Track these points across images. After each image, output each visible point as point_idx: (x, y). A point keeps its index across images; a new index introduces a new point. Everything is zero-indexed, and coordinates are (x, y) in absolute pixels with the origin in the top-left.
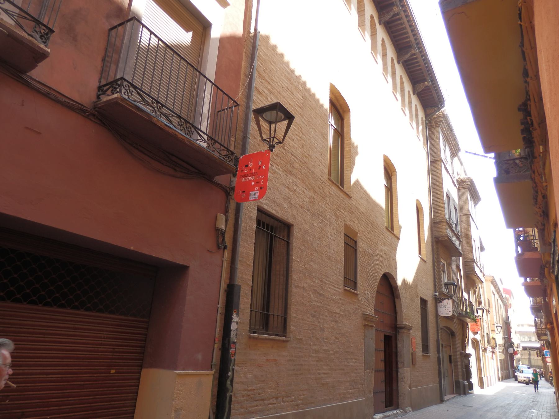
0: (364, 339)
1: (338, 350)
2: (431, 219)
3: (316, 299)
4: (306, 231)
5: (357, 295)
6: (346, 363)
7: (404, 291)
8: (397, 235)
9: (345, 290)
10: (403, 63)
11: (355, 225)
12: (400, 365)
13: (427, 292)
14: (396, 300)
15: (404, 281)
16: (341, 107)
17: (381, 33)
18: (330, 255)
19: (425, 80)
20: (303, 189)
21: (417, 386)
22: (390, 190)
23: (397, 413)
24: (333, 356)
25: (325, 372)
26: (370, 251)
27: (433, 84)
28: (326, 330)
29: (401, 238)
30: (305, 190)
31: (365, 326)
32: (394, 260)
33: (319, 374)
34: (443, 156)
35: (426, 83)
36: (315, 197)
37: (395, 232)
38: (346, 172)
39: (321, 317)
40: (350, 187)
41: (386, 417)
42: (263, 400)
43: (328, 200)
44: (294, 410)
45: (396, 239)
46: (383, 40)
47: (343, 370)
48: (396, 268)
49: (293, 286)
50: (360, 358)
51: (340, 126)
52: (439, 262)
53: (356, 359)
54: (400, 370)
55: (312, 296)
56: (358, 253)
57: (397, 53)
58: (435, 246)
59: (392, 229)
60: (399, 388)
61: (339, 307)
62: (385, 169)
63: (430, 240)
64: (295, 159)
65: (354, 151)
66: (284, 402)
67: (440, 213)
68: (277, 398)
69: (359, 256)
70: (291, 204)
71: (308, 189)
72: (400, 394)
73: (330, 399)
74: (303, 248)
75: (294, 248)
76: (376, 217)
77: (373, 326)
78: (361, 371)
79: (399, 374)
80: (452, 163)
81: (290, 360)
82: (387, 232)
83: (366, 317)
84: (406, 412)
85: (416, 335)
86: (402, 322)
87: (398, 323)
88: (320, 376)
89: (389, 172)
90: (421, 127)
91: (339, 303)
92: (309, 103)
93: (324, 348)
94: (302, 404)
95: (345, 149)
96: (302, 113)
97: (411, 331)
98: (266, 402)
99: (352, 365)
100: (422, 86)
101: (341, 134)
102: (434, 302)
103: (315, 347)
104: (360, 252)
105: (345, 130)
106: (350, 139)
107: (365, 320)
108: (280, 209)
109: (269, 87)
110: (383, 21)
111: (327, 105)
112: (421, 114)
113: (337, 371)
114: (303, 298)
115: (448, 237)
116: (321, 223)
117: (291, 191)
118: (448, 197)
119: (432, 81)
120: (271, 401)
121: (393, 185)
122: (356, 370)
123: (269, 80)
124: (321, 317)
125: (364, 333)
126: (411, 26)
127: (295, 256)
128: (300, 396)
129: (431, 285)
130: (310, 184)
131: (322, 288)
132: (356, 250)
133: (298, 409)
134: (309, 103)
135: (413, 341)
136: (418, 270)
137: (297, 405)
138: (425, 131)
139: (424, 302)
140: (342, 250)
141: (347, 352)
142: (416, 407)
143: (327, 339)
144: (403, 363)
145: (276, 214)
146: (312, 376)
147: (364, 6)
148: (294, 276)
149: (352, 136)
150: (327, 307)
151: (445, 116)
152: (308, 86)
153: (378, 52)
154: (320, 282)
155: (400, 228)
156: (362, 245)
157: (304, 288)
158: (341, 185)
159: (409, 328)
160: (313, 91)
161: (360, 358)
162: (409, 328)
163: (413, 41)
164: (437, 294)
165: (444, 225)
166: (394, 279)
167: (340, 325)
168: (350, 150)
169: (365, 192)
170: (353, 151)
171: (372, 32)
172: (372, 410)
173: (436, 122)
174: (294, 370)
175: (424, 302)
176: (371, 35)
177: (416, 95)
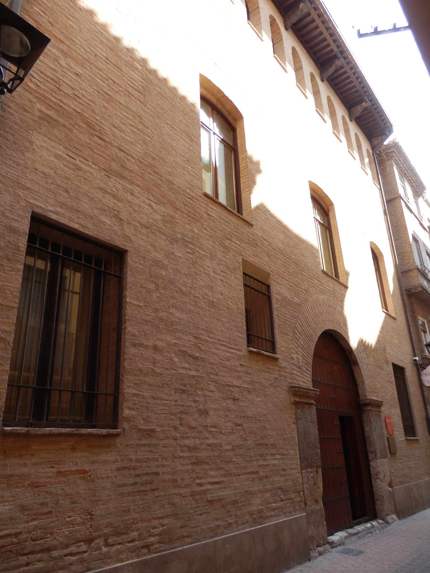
0: (296, 423)
1: (242, 443)
2: (396, 266)
3: (187, 366)
4: (157, 263)
5: (277, 359)
6: (261, 462)
7: (364, 355)
8: (345, 284)
9: (250, 352)
10: (327, 80)
11: (263, 262)
12: (371, 456)
13: (405, 357)
14: (354, 368)
15: (362, 343)
16: (230, 114)
17: (325, 90)
18: (215, 300)
19: (361, 101)
20: (148, 201)
21: (402, 483)
22: (327, 227)
23: (373, 526)
24: (231, 454)
25: (216, 480)
26: (296, 300)
27: (373, 105)
28: (211, 413)
29: (349, 285)
30: (153, 204)
31: (296, 403)
32: (341, 313)
33: (200, 485)
34: (401, 192)
35: (364, 104)
36: (177, 216)
37: (341, 280)
38: (244, 195)
39: (199, 393)
40: (251, 211)
41: (351, 535)
42: (49, 550)
43: (205, 223)
44: (138, 556)
45: (342, 288)
46: (356, 134)
47: (257, 473)
48: (346, 325)
49: (127, 344)
50: (292, 452)
51: (231, 137)
52: (415, 320)
53: (283, 454)
54: (372, 463)
55: (176, 360)
56: (274, 301)
57: (319, 69)
58: (406, 298)
59: (336, 275)
60: (374, 489)
61: (240, 378)
62: (314, 199)
63: (398, 292)
64: (129, 157)
65: (256, 168)
66: (107, 545)
67: (408, 259)
68: (89, 541)
69: (275, 305)
70: (121, 219)
71: (159, 202)
72: (376, 496)
73: (230, 524)
74: (152, 286)
75: (129, 285)
76: (303, 256)
77: (312, 404)
78: (294, 471)
79: (371, 468)
80: (417, 203)
81: (124, 468)
82: (325, 277)
83: (296, 391)
84: (387, 523)
85: (392, 412)
86: (366, 396)
87: (361, 398)
88: (203, 488)
89: (322, 204)
90: (367, 160)
91: (239, 372)
92: (157, 89)
93: (208, 442)
94: (159, 542)
95: (241, 166)
96: (142, 99)
97: (383, 408)
98: (55, 553)
99: (274, 465)
100: (359, 110)
101: (233, 145)
102: (415, 369)
103: (187, 442)
104: (277, 300)
105: (239, 141)
106: (246, 151)
107: (295, 395)
108: (93, 223)
109: (65, 48)
110: (326, 77)
111: (194, 98)
112: (365, 145)
113: (243, 477)
114: (154, 363)
115: (422, 287)
116: (193, 253)
117: (120, 201)
118: (416, 240)
119: (371, 101)
120: (73, 549)
121: (331, 221)
122: (285, 470)
123: (62, 39)
124: (199, 393)
125: (296, 414)
126: (327, 29)
127: (130, 297)
128: (155, 527)
129: (407, 348)
130: (163, 197)
131: (200, 349)
132: (269, 298)
133: (292, 516)
134: (157, 89)
135: (388, 421)
136: (383, 328)
137: (147, 546)
138: (374, 165)
139: (398, 371)
140: (242, 295)
141: (260, 445)
142: (402, 513)
143: (215, 427)
144: (375, 452)
145: (82, 230)
146: (183, 491)
147: (301, 61)
148: (129, 329)
149: (248, 148)
150: (212, 376)
151: (395, 145)
152: (153, 64)
153: (340, 131)
154: (193, 339)
155: (347, 274)
156: (279, 290)
157: (155, 348)
158: (238, 212)
159: (378, 405)
160: (163, 73)
161: (292, 452)
162: (378, 405)
163: (335, 49)
164: (417, 358)
165: (415, 273)
166: (346, 340)
167: (242, 404)
168: (247, 167)
169: (279, 222)
170: (251, 166)
171: (295, 64)
172: (323, 529)
173: (387, 154)
174: (135, 484)
175: (398, 371)
176: (331, 116)
177: (354, 122)
